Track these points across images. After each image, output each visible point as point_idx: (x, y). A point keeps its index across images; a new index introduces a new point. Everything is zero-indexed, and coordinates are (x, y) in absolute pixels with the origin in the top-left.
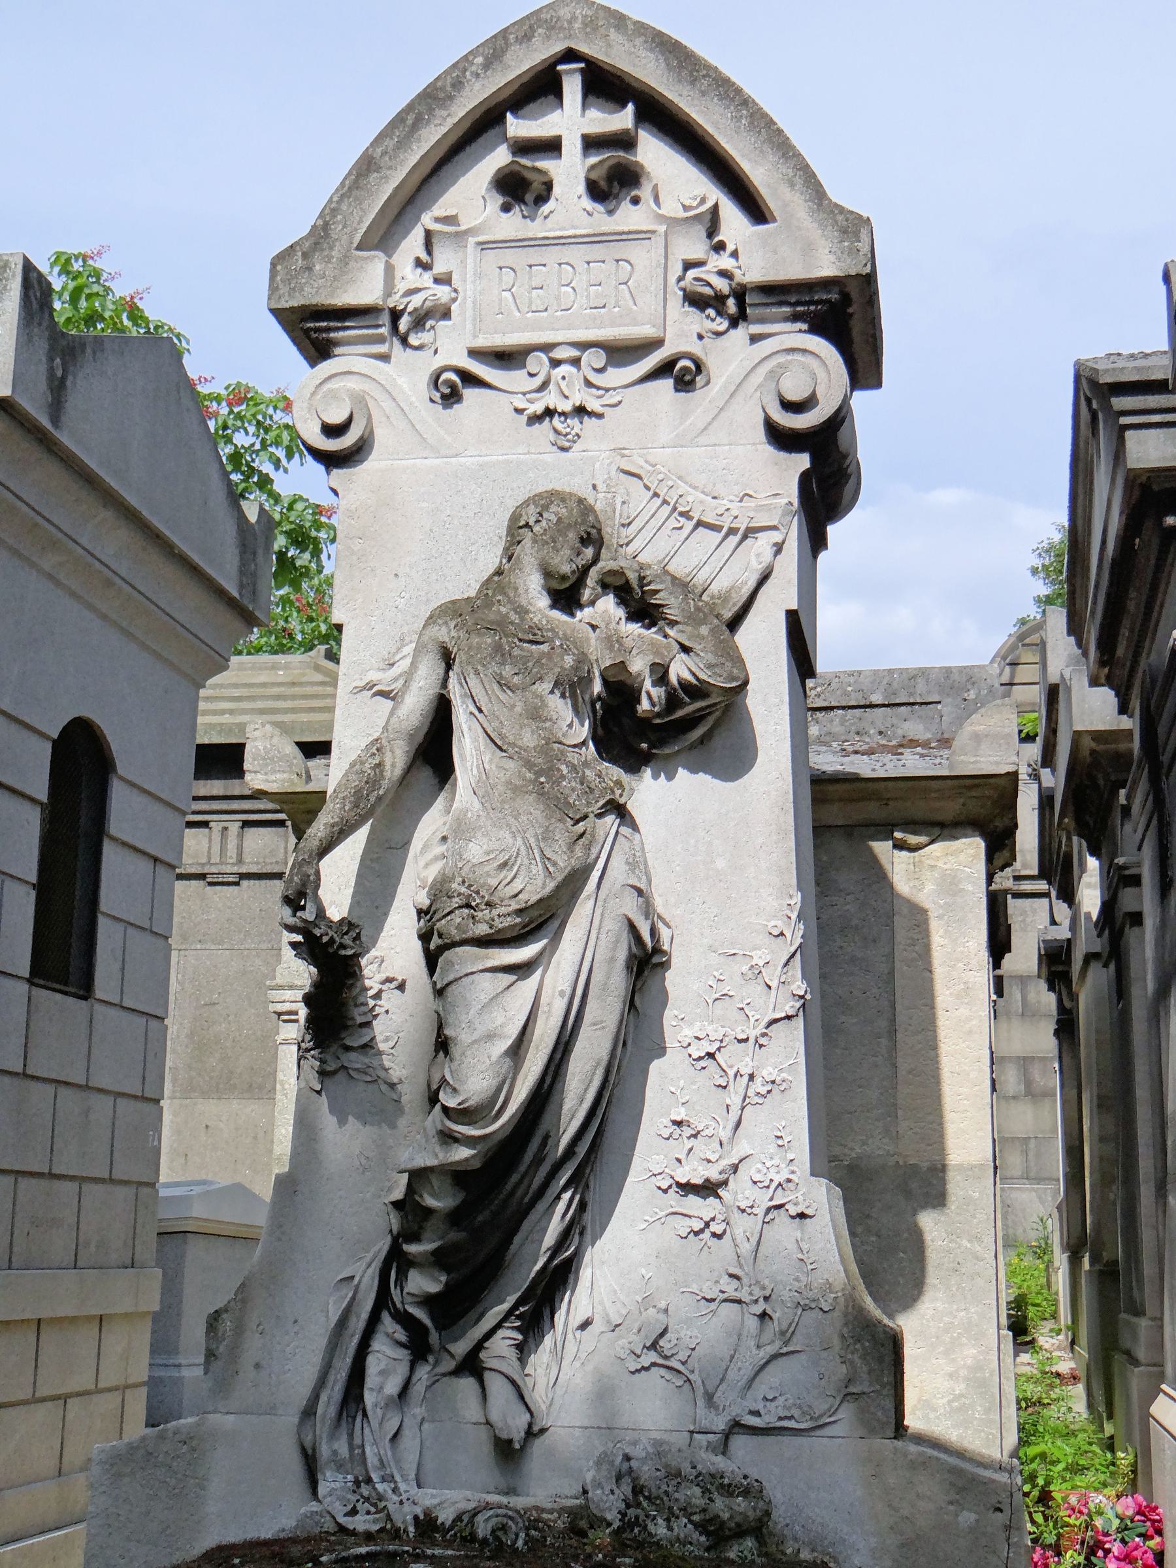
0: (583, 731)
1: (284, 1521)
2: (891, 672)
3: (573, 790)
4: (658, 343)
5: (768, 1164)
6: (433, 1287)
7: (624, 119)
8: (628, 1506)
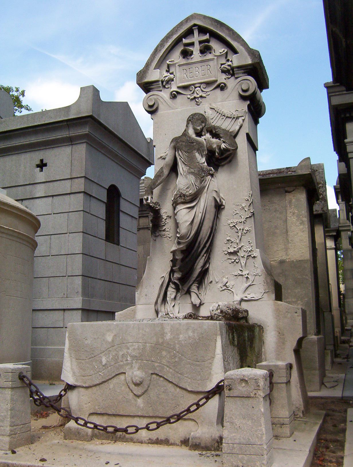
0: (204, 160)
4: (216, 81)
7: (207, 37)
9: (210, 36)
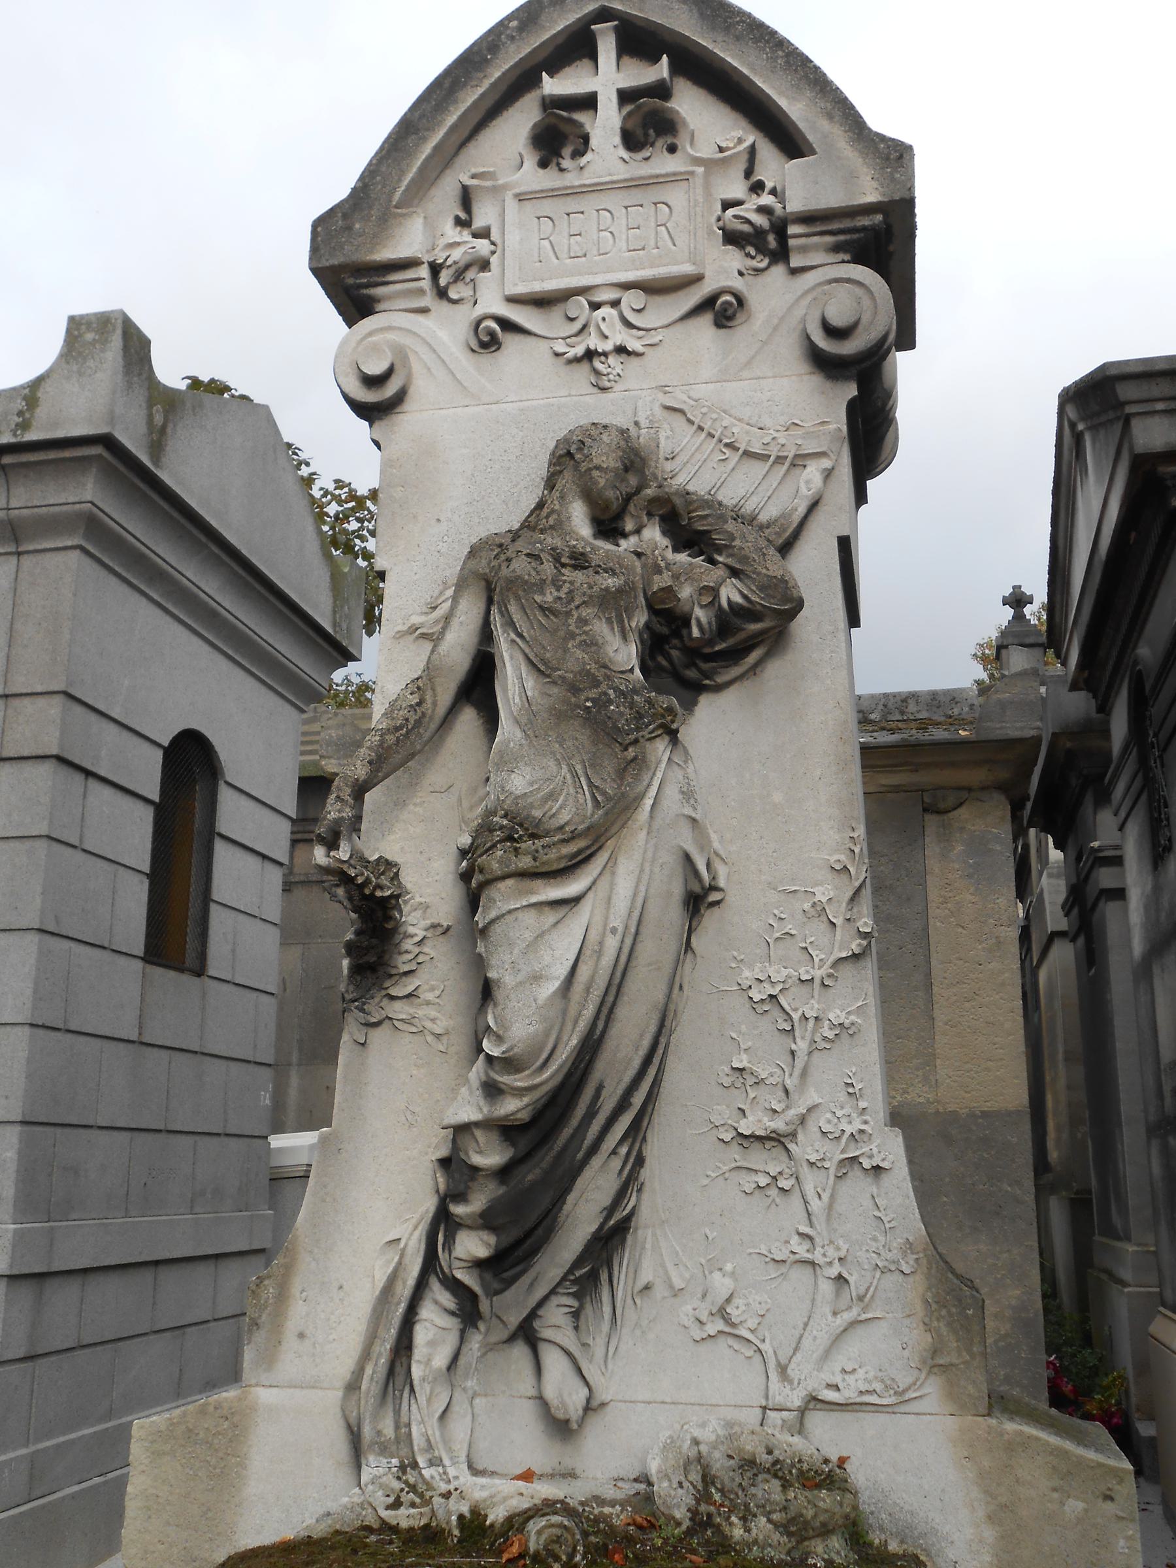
1: (329, 1504)
2: (886, 695)
3: (622, 714)
4: (698, 279)
5: (839, 1113)
6: (482, 1252)
7: (662, 69)
8: (698, 1501)
9: (675, 69)
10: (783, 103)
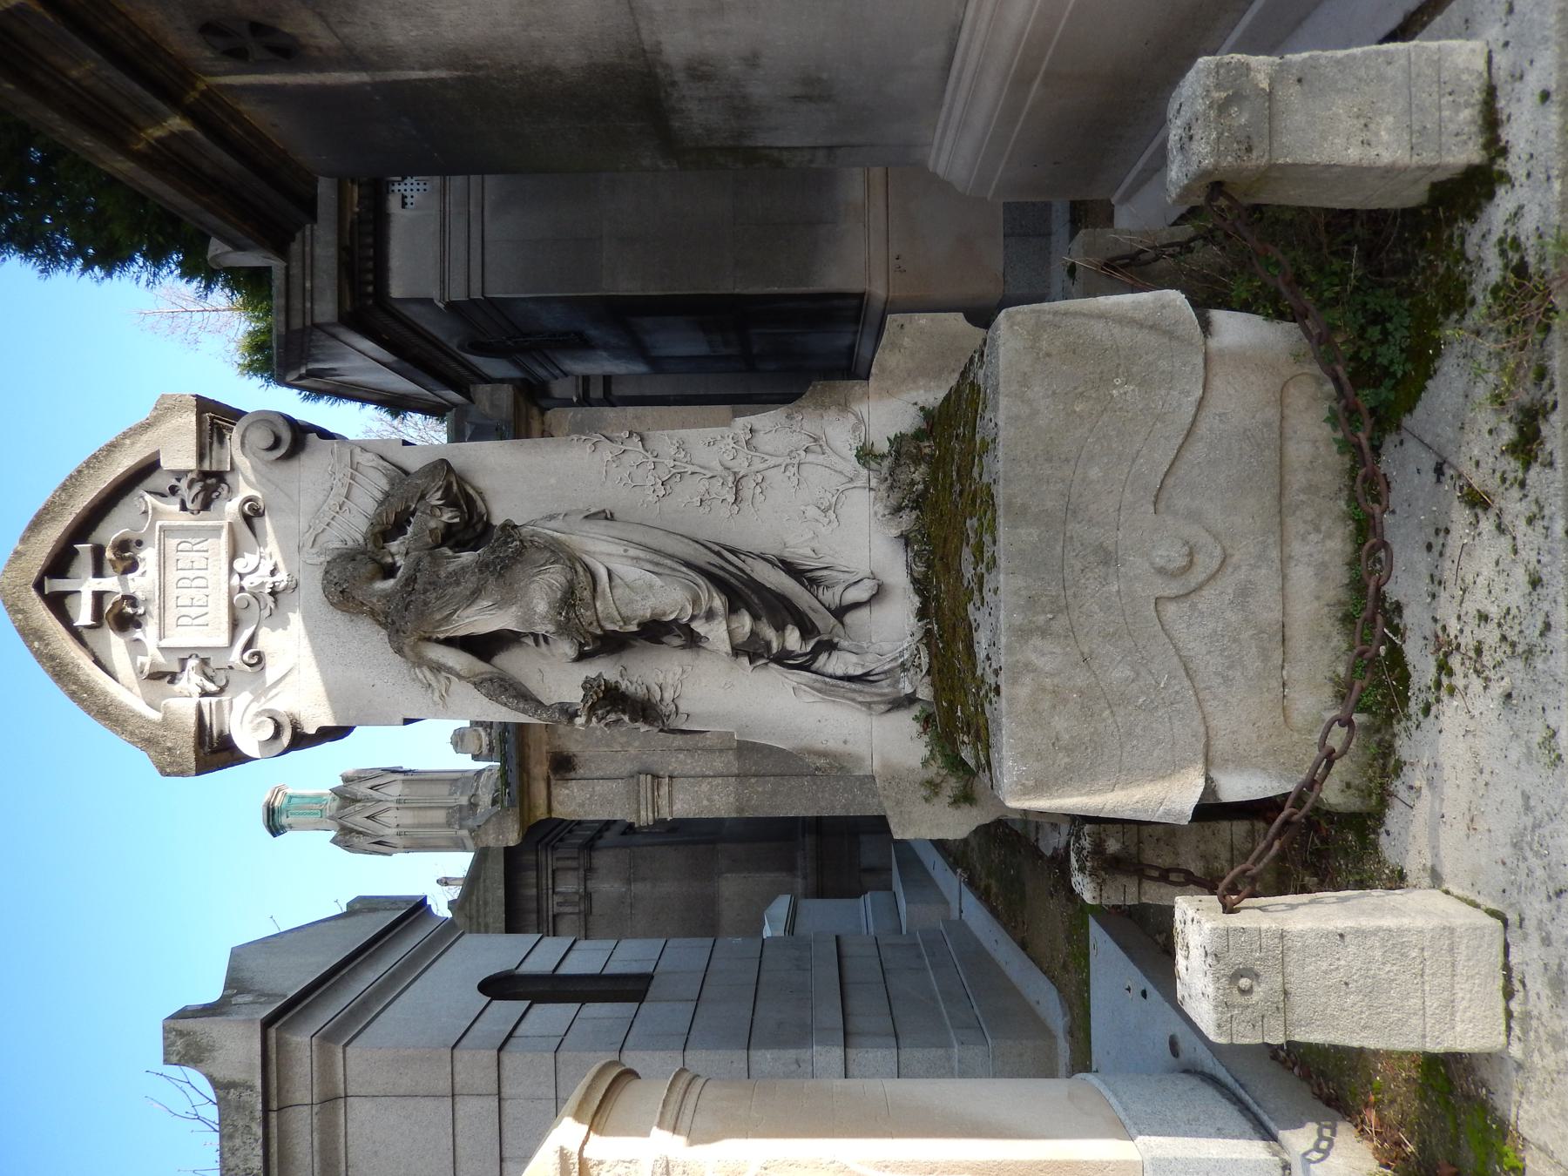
6: (797, 633)
7: (84, 548)
10: (121, 470)
